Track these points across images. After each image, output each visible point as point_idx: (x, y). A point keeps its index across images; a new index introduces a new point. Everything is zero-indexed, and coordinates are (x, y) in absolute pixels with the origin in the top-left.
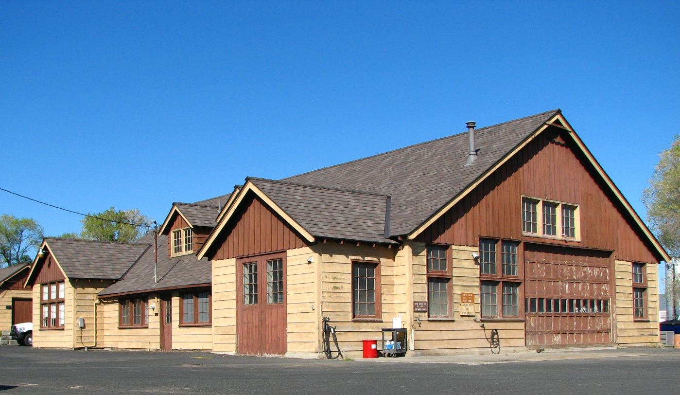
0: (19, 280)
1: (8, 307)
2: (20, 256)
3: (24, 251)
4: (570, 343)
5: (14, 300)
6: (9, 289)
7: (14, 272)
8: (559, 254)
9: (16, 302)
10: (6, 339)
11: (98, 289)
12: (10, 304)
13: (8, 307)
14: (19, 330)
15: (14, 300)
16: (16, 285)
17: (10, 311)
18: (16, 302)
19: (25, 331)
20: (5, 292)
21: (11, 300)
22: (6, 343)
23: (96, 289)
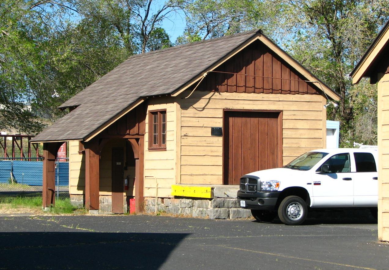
0: (239, 70)
1: (215, 132)
2: (149, 29)
3: (156, 18)
4: (182, 204)
5: (228, 114)
6: (217, 90)
7: (230, 49)
8: (388, 69)
9: (231, 120)
10: (223, 206)
11: (154, 105)
12: (219, 124)
13: (215, 132)
14: (265, 187)
15: (228, 114)
16: (231, 81)
17: (220, 140)
18: (231, 120)
19: (281, 189)
20: (208, 96)
21: (220, 114)
22: (223, 216)
23: (173, 103)
